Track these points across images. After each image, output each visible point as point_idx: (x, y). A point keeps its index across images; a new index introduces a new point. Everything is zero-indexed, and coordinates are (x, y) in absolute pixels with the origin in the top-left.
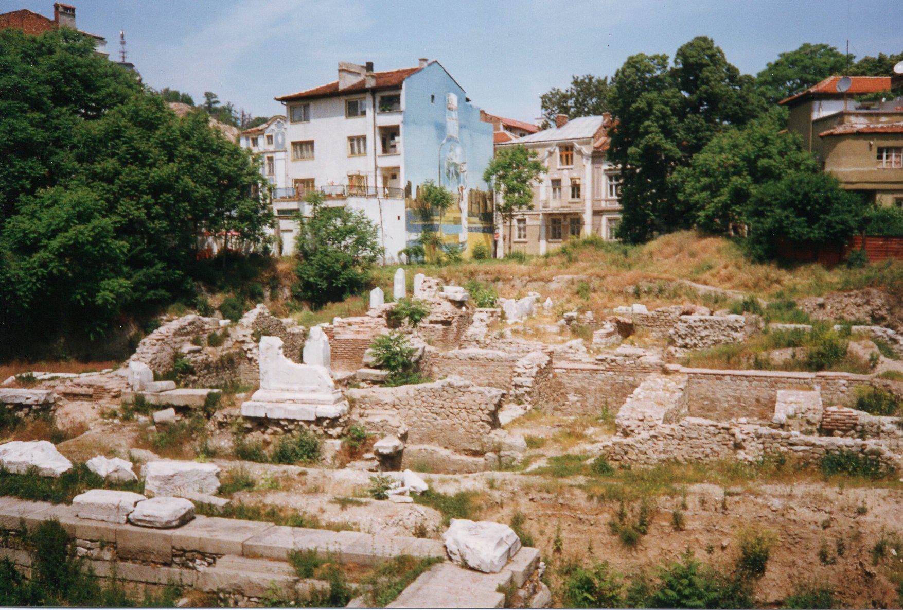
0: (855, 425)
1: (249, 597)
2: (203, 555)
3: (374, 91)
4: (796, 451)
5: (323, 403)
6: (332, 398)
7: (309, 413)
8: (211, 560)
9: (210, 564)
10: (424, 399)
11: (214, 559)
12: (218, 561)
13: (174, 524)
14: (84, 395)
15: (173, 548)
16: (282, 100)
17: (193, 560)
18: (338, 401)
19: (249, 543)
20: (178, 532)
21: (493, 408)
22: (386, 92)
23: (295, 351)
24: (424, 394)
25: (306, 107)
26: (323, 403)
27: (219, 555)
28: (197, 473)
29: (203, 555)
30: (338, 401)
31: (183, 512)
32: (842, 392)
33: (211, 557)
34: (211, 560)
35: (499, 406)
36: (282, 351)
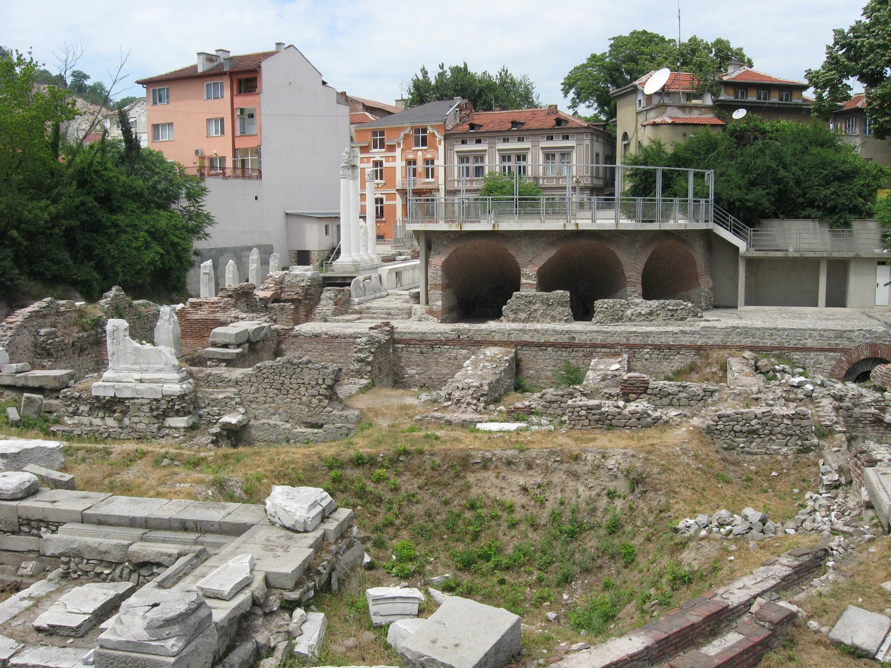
0: (20, 221)
1: (88, 560)
2: (47, 524)
3: (231, 74)
4: (594, 415)
5: (165, 381)
6: (177, 376)
7: (155, 391)
8: (54, 528)
9: (53, 532)
10: (265, 376)
11: (57, 527)
12: (60, 528)
13: (20, 495)
14: (157, 529)
15: (19, 518)
16: (138, 82)
17: (39, 529)
18: (182, 380)
19: (88, 512)
20: (23, 503)
21: (329, 382)
22: (244, 76)
23: (143, 331)
24: (265, 371)
25: (769, 91)
26: (165, 381)
27: (58, 524)
28: (42, 449)
29: (47, 524)
30: (182, 380)
31: (27, 484)
32: (646, 360)
33: (53, 525)
34: (54, 528)
35: (336, 381)
36: (127, 333)
